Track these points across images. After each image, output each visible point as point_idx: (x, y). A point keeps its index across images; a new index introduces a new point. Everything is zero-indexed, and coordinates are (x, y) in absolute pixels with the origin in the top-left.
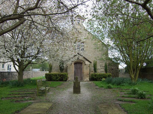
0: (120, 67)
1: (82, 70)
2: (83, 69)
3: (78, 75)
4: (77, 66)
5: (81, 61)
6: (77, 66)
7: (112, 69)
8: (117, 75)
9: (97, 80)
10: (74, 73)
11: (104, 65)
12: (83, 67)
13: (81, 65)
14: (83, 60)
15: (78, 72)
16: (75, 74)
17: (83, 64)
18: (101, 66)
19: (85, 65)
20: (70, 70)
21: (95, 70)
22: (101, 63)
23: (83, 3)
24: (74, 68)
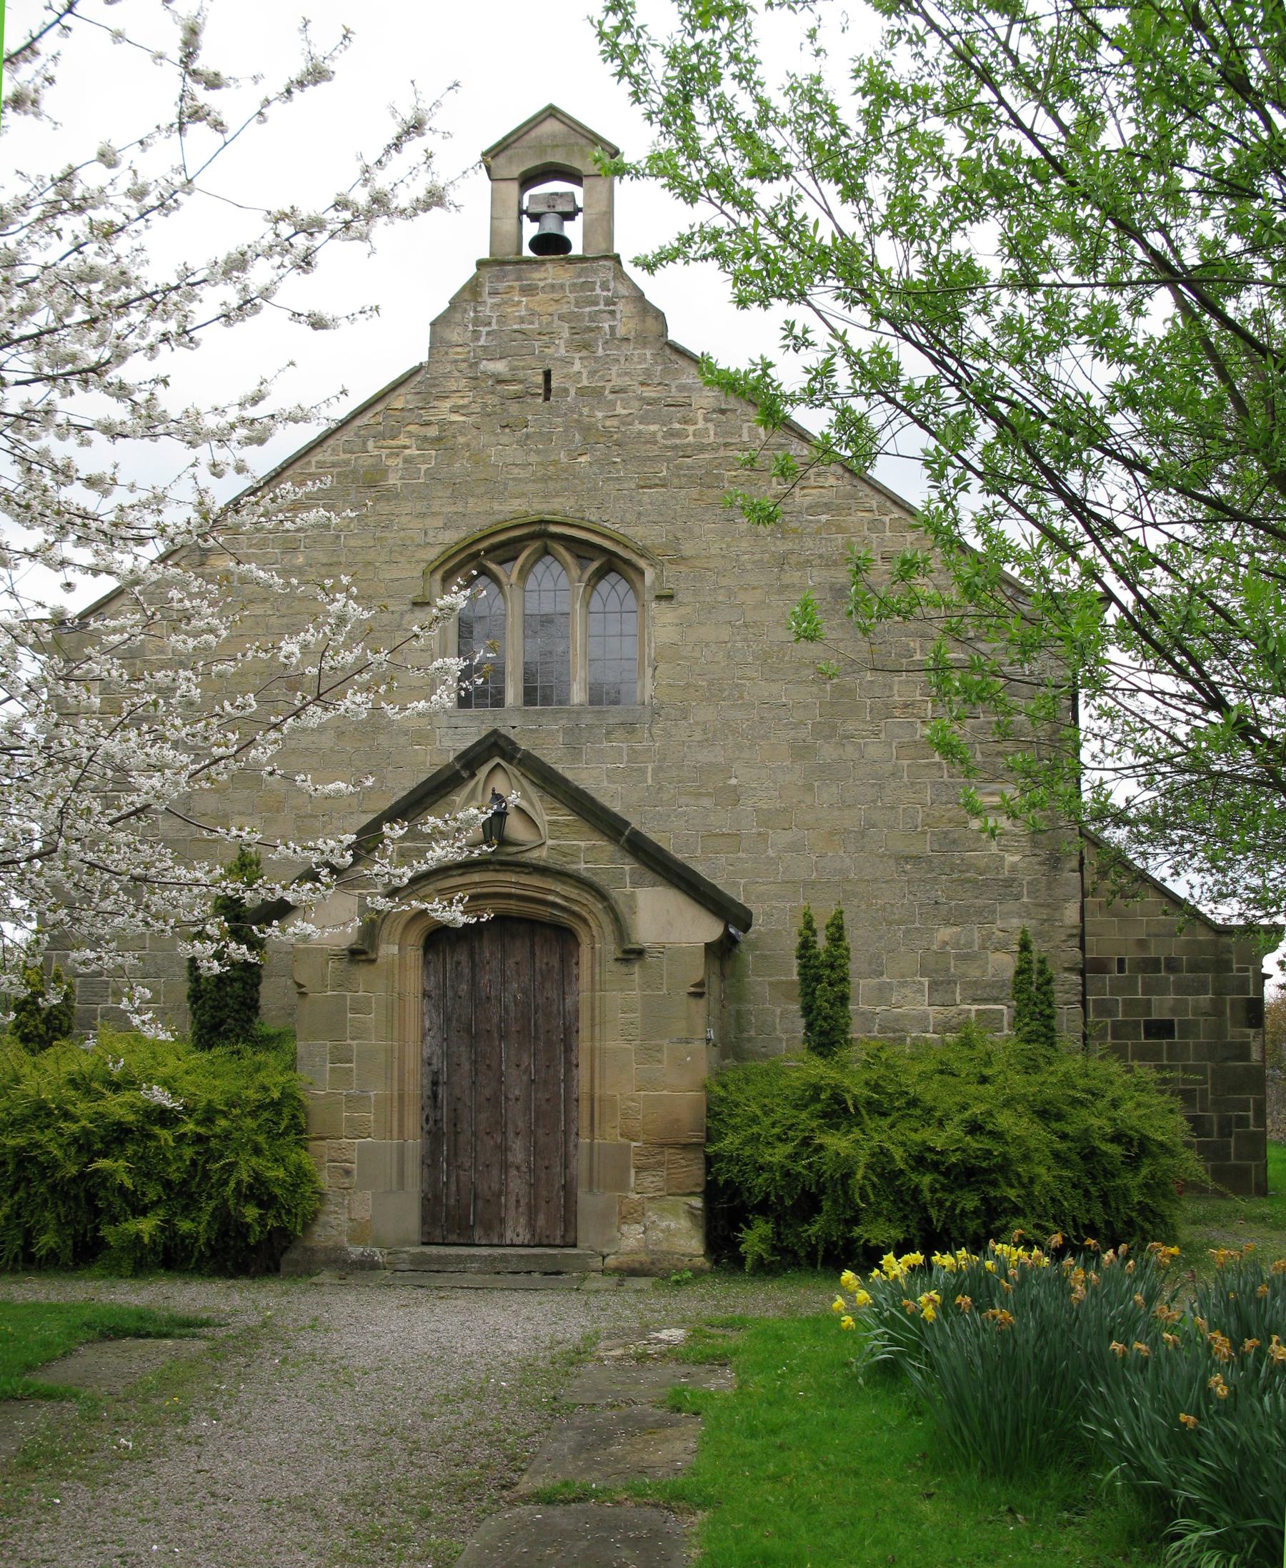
0: (1139, 392)
1: (571, 1066)
2: (584, 1033)
3: (504, 1149)
4: (474, 983)
5: (559, 892)
6: (474, 983)
7: (1161, 1029)
8: (1242, 1122)
9: (166, 1336)
10: (413, 1121)
11: (1004, 964)
12: (585, 996)
13: (547, 958)
14: (581, 867)
15: (494, 1101)
16: (434, 1135)
17: (584, 939)
18: (940, 986)
19: (632, 955)
20: (341, 1056)
21: (472, 956)
22: (945, 933)
23: (1111, 692)
24: (415, 1014)
